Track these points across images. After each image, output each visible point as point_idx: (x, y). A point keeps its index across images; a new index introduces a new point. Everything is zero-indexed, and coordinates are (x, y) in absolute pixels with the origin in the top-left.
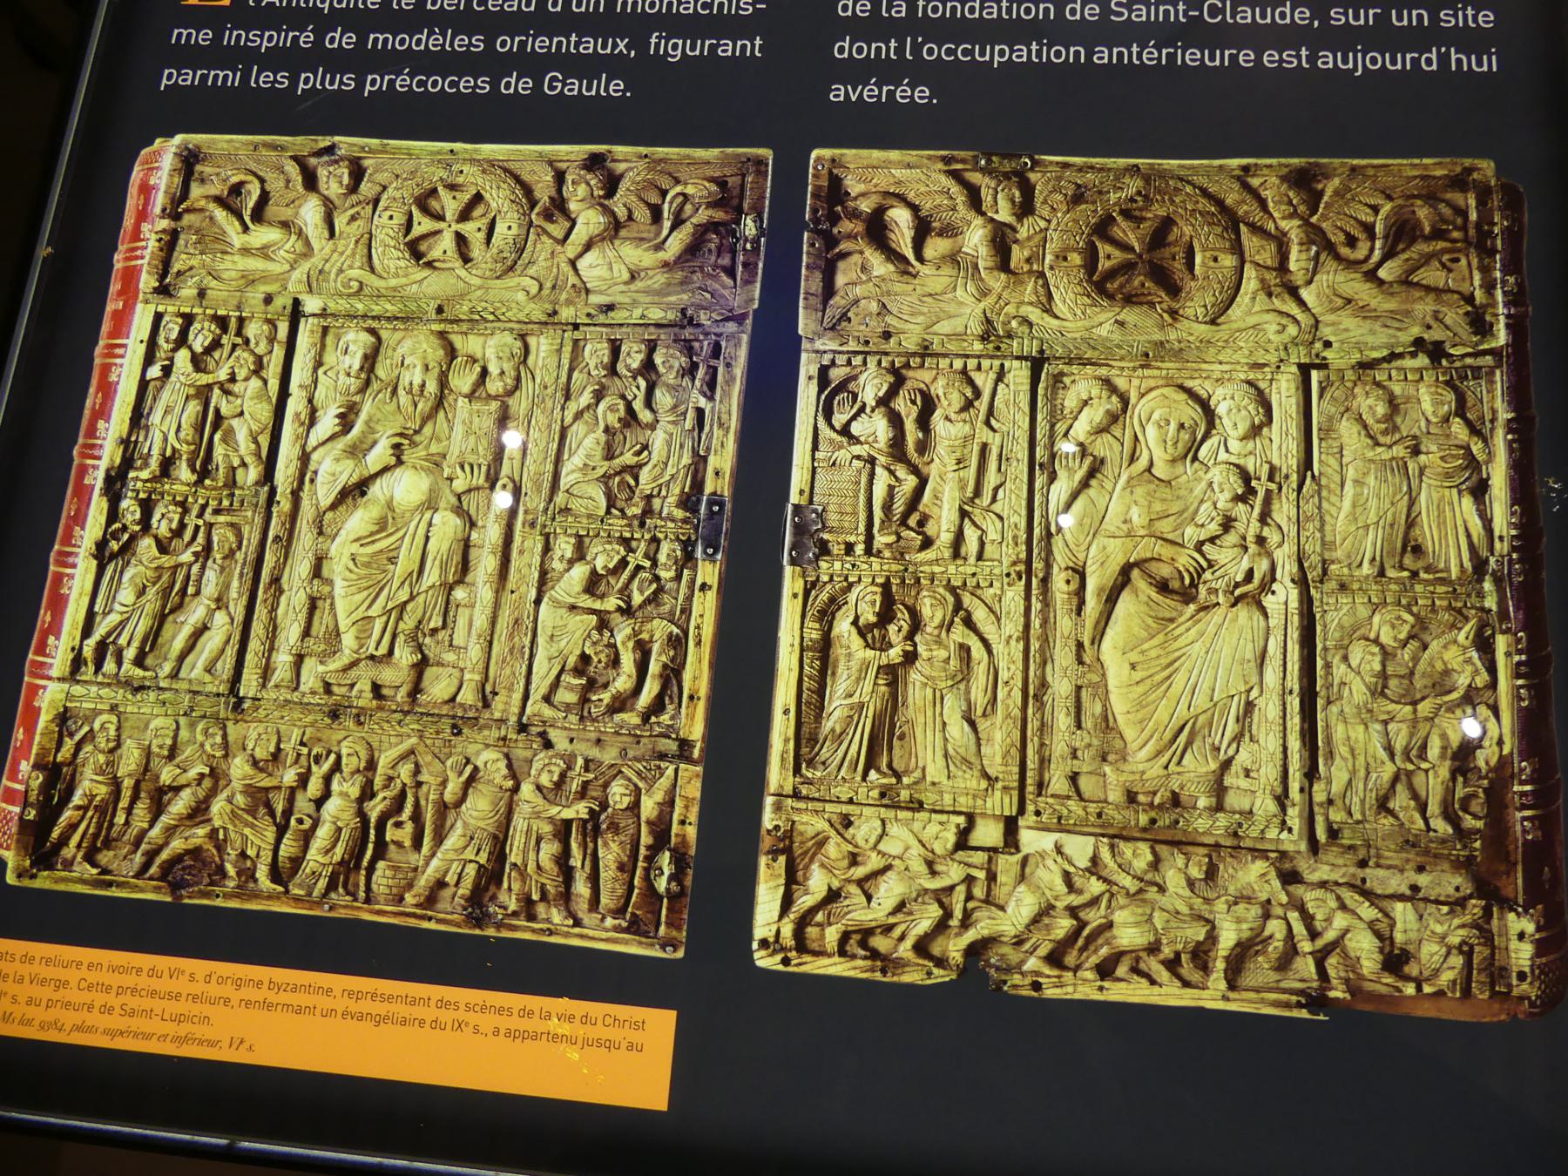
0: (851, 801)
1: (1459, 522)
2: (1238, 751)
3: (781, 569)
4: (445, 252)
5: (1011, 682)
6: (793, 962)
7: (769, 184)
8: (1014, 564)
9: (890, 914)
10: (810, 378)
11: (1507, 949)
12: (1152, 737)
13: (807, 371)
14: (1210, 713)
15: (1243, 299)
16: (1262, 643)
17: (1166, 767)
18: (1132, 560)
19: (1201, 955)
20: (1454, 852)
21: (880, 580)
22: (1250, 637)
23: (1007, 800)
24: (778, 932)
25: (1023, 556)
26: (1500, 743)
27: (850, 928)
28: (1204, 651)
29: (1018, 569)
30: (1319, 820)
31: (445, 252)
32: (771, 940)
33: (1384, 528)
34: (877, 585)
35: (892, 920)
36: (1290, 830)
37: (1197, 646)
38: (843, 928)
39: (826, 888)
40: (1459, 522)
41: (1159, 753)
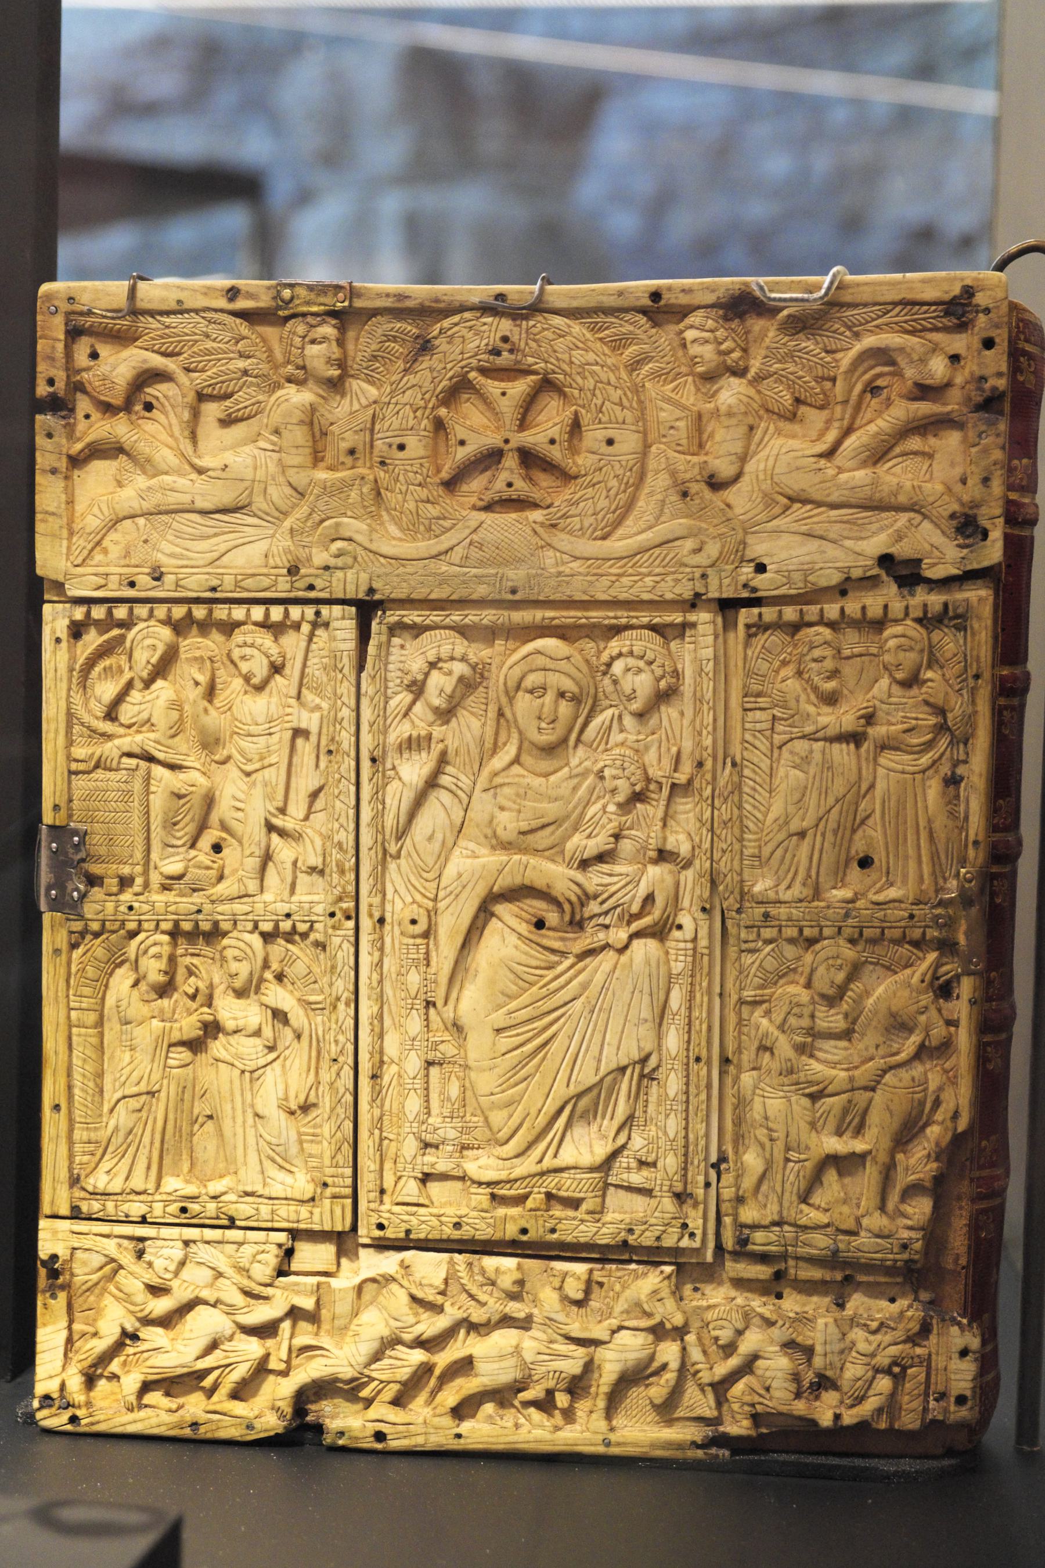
0: (144, 1221)
1: (922, 823)
2: (629, 1138)
3: (40, 914)
4: (462, 443)
5: (341, 1059)
6: (83, 1422)
7: (943, 274)
8: (340, 899)
9: (197, 1358)
10: (58, 640)
11: (946, 1369)
12: (520, 1125)
13: (53, 631)
14: (595, 1092)
15: (645, 505)
16: (662, 997)
17: (540, 1161)
18: (496, 889)
19: (577, 1386)
20: (891, 1256)
21: (166, 926)
22: (646, 990)
23: (338, 1212)
24: (63, 1387)
25: (351, 888)
26: (956, 1116)
27: (151, 1378)
28: (587, 1010)
29: (345, 905)
30: (727, 1220)
31: (462, 443)
32: (55, 1395)
33: (823, 835)
34: (163, 932)
35: (202, 1364)
36: (692, 1235)
37: (578, 1004)
38: (142, 1377)
39: (118, 1330)
40: (922, 823)
41: (530, 1146)
